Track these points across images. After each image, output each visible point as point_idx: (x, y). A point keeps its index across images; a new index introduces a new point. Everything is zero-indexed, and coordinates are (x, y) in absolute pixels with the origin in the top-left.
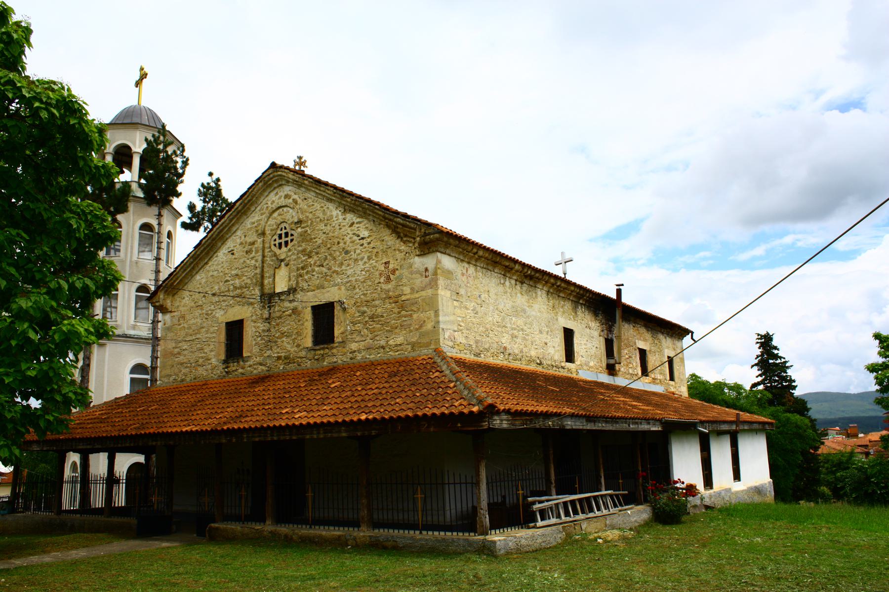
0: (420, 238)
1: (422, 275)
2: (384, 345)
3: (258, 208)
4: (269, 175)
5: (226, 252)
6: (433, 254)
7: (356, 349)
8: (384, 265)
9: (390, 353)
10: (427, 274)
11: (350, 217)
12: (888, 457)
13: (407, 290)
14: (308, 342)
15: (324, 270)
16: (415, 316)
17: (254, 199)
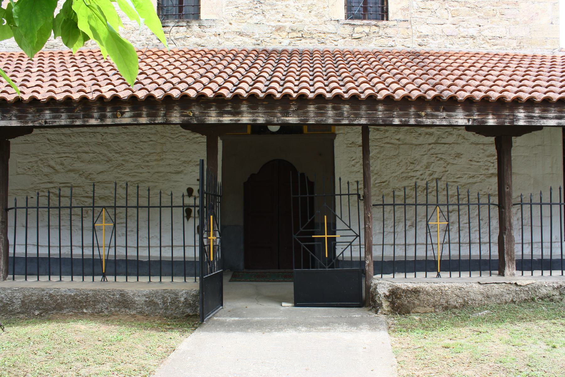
2: (475, 35)
12: (365, 2)
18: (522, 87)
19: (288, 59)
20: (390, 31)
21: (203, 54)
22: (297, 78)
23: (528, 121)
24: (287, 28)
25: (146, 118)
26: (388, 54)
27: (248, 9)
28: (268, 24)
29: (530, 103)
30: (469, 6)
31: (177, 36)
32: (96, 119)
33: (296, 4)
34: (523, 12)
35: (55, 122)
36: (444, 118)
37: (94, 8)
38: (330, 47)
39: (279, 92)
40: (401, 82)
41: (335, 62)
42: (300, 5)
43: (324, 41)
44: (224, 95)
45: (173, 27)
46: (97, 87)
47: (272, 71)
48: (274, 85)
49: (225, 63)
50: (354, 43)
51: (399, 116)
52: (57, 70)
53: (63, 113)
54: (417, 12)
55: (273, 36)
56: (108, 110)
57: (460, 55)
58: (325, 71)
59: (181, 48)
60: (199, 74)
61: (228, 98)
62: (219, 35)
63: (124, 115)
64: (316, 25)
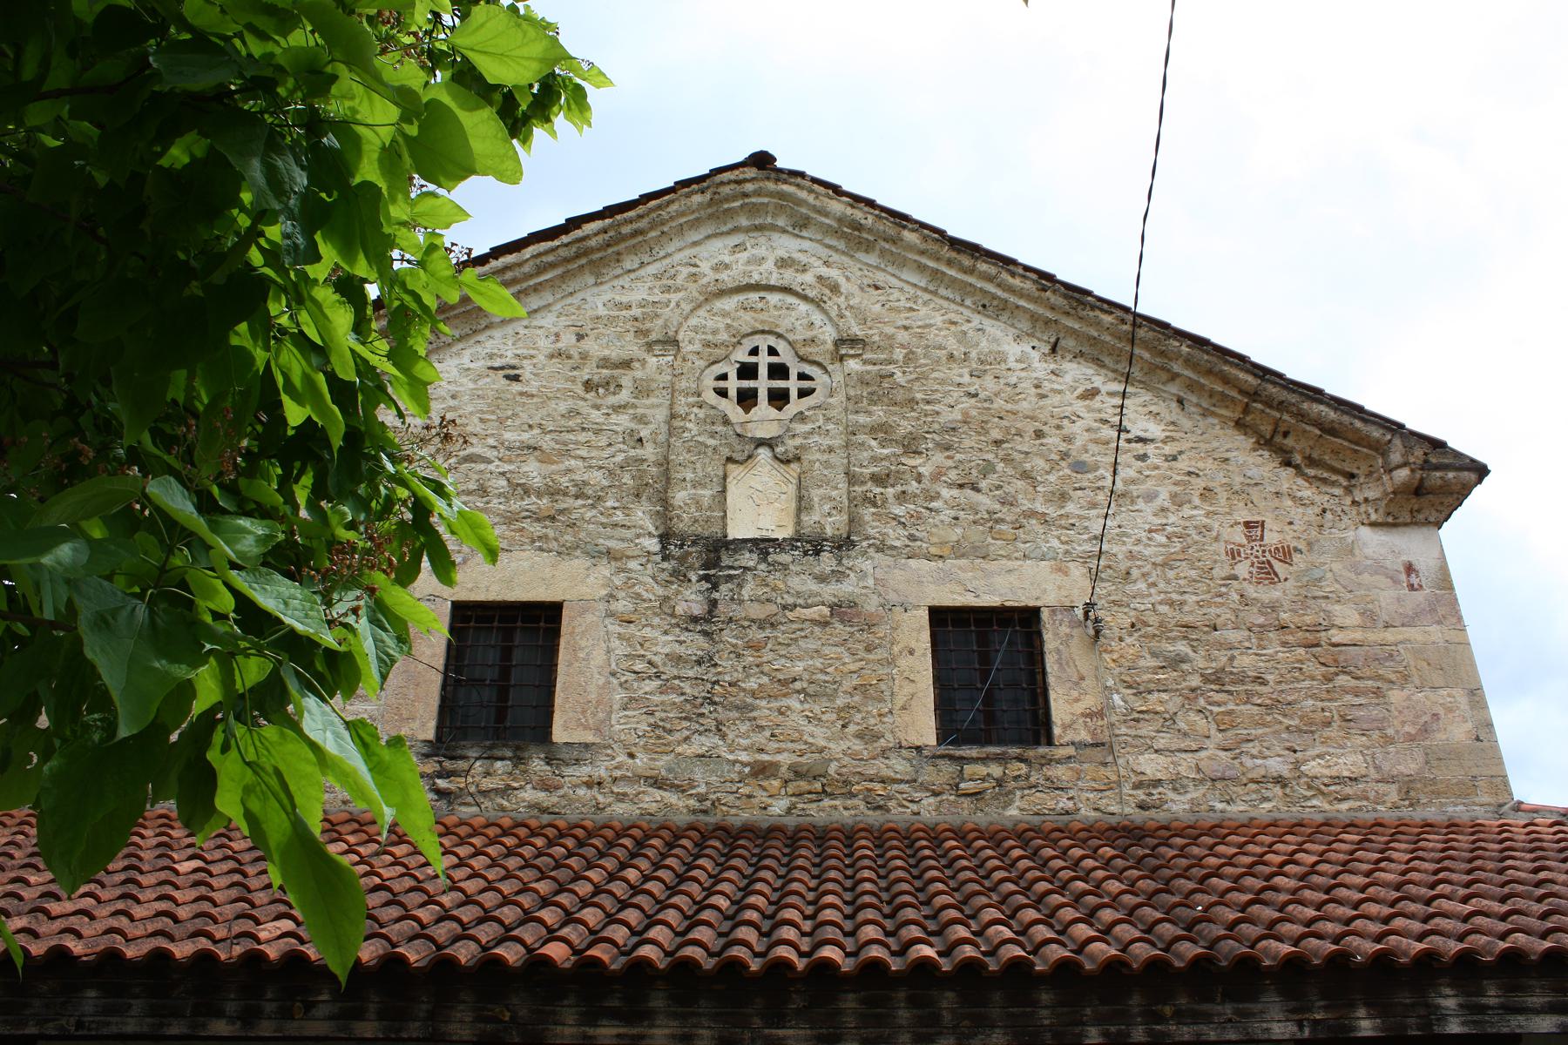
0: (1412, 471)
1: (1396, 582)
2: (1286, 774)
3: (651, 269)
4: (738, 182)
5: (480, 365)
6: (1424, 530)
7: (1159, 776)
8: (1241, 528)
9: (1314, 802)
10: (1414, 580)
11: (1076, 373)
13: (1346, 614)
14: (923, 727)
15: (985, 501)
16: (1396, 696)
17: (653, 234)
18: (1437, 920)
19: (785, 855)
20: (1060, 772)
21: (551, 836)
22: (809, 910)
23: (1474, 1022)
24: (784, 769)
25: (376, 1024)
26: (1057, 834)
27: (680, 718)
28: (731, 757)
29: (1467, 969)
30: (1259, 701)
31: (487, 784)
32: (231, 1020)
33: (806, 706)
34: (1400, 712)
35: (108, 1024)
36: (1230, 1020)
37: (266, 773)
38: (899, 814)
39: (756, 955)
40: (1099, 920)
41: (913, 862)
42: (817, 709)
43: (882, 803)
44: (604, 962)
45: (477, 759)
46: (247, 925)
47: (740, 889)
48: (745, 933)
49: (610, 863)
50: (965, 805)
51: (1099, 1021)
52: (145, 868)
53: (137, 997)
54: (1125, 721)
55: (744, 790)
56: (269, 995)
57: (1250, 829)
58: (887, 889)
59: (493, 815)
60: (535, 895)
61: (614, 971)
62: (599, 784)
63: (314, 1011)
64: (862, 760)
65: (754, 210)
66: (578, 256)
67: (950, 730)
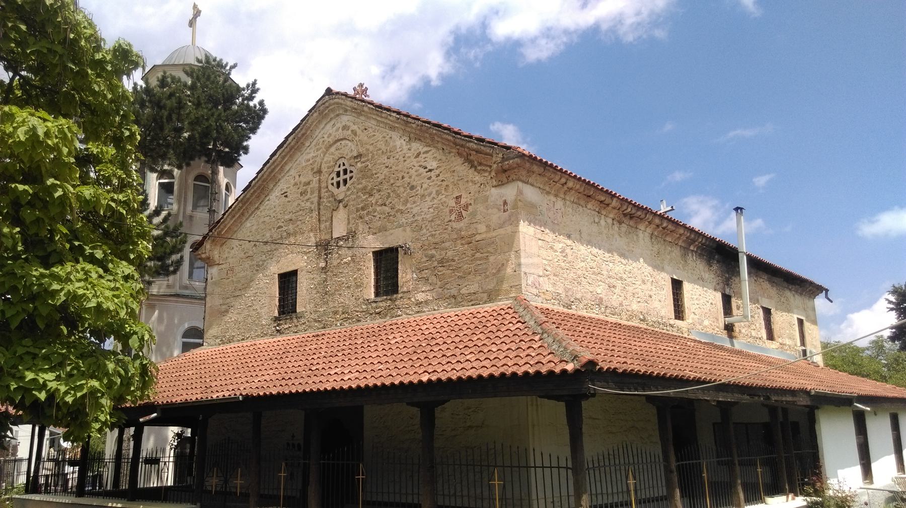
1: (499, 210)
16: (492, 259)
65: (332, 110)
66: (291, 149)
67: (377, 294)
